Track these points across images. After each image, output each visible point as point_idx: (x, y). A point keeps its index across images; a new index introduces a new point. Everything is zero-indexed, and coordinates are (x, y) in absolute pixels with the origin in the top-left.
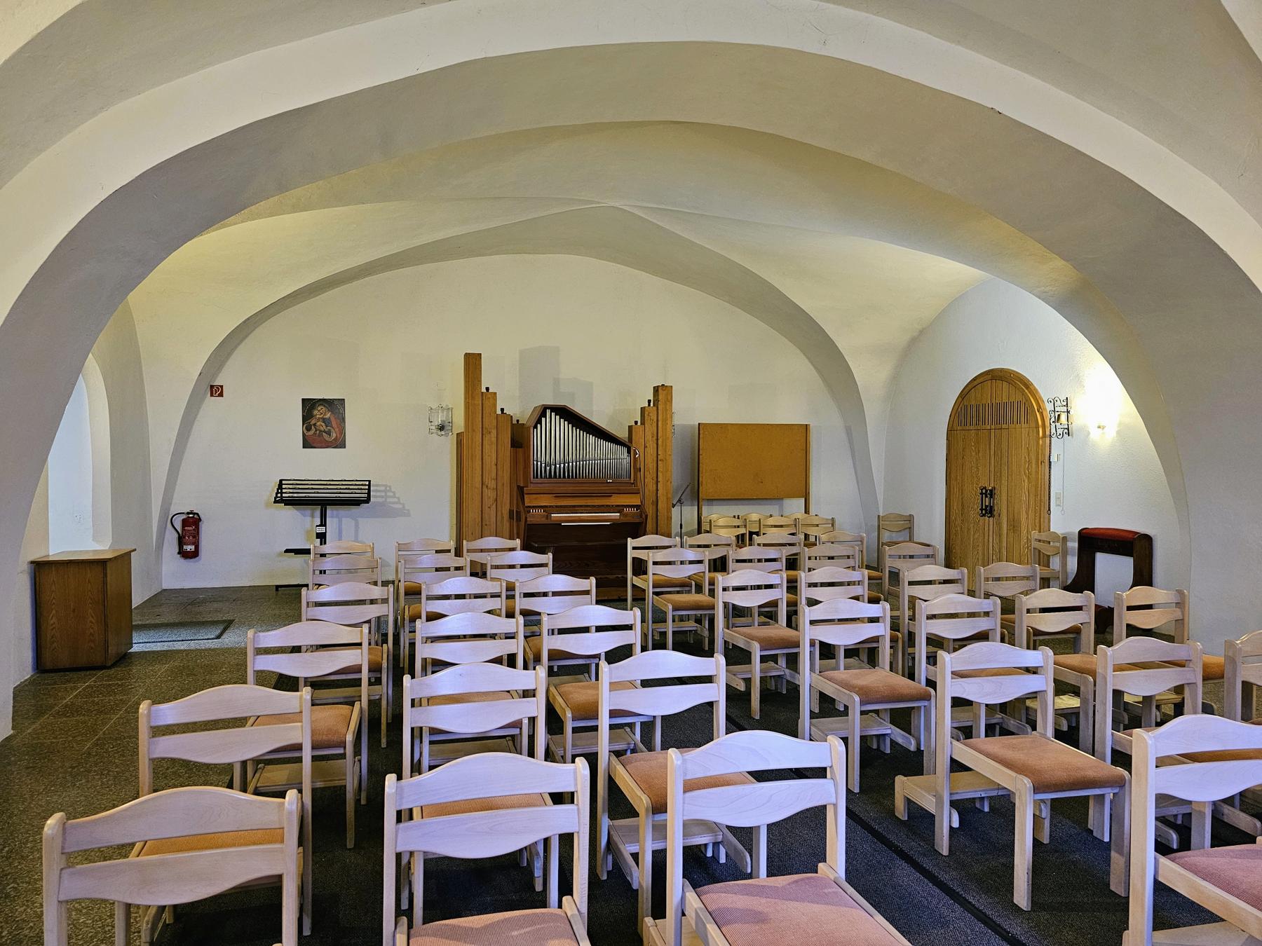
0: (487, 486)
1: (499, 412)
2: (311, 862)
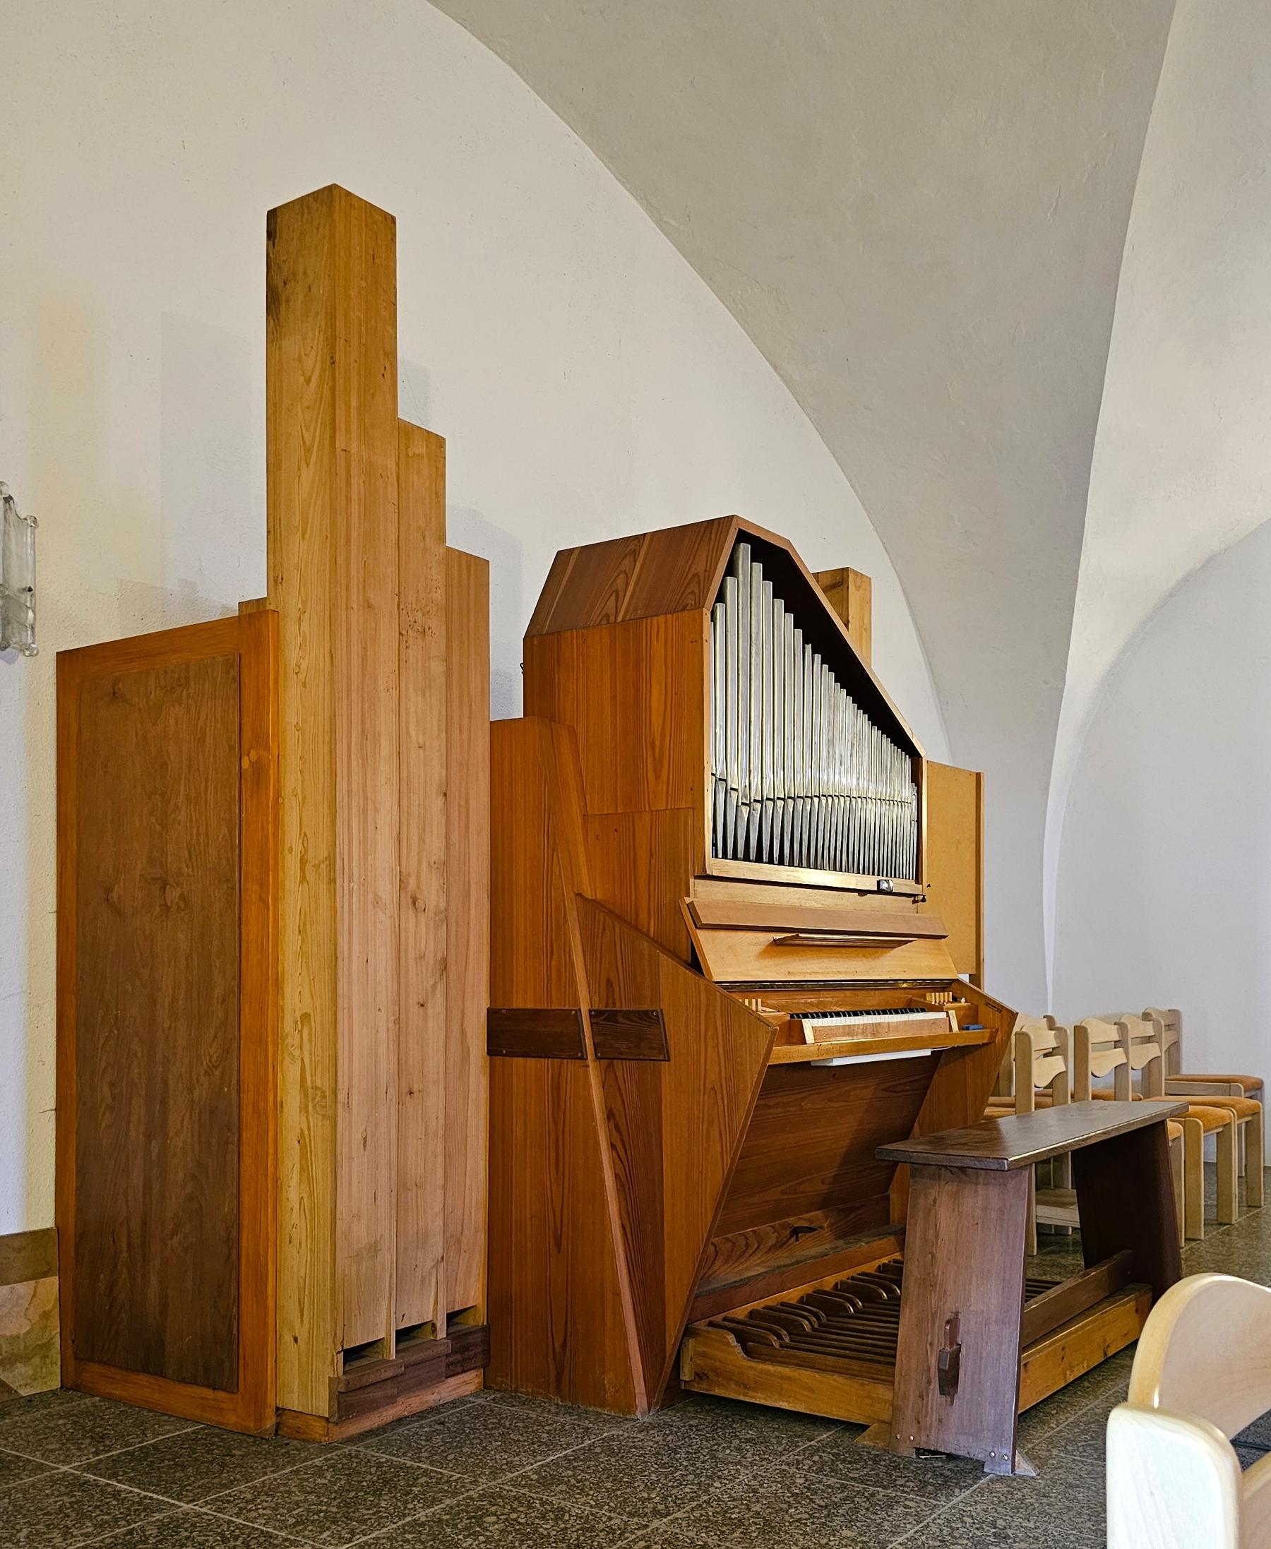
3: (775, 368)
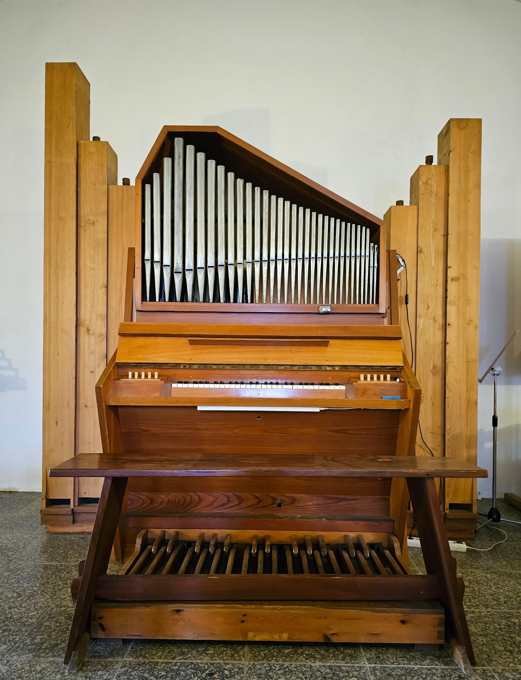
0: (88, 330)
1: (120, 183)
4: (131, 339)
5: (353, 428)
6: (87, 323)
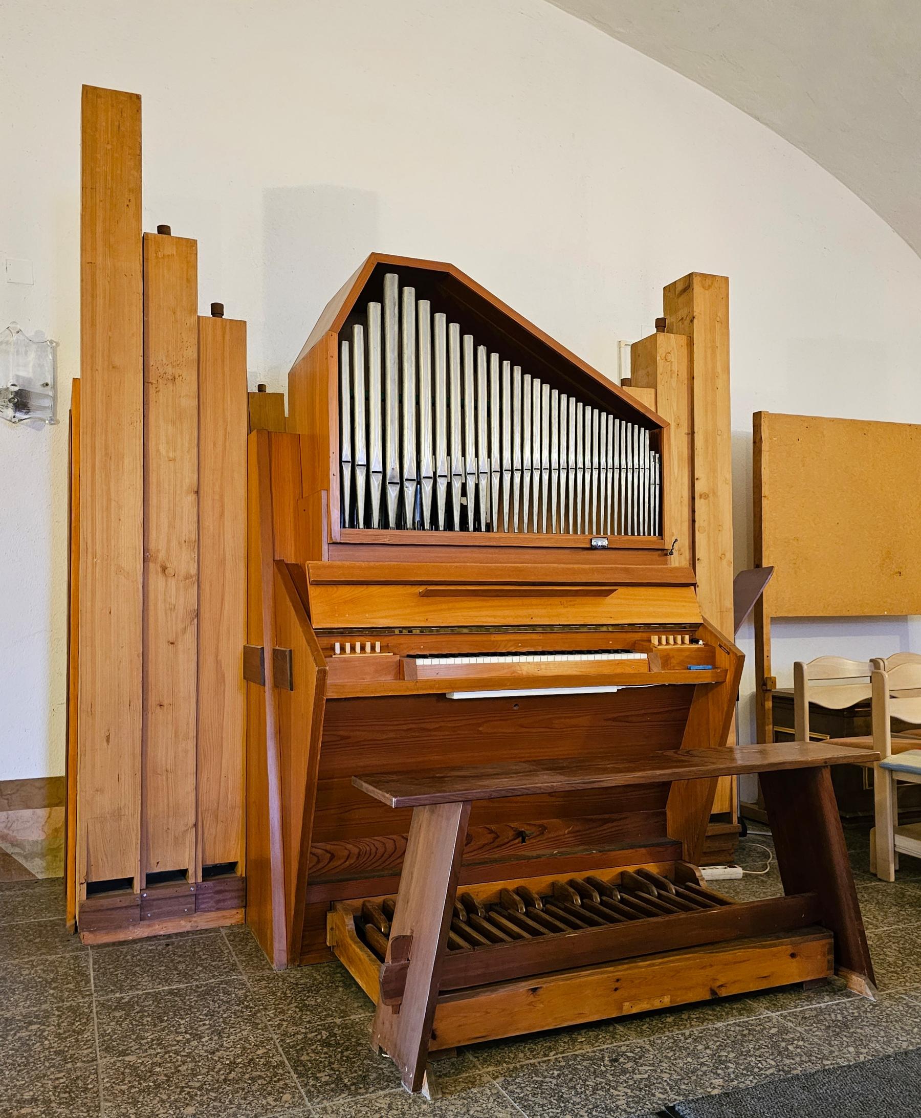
0: (164, 569)
1: (204, 311)
2: (314, 805)
3: (758, 119)
4: (330, 589)
5: (637, 713)
6: (162, 555)
